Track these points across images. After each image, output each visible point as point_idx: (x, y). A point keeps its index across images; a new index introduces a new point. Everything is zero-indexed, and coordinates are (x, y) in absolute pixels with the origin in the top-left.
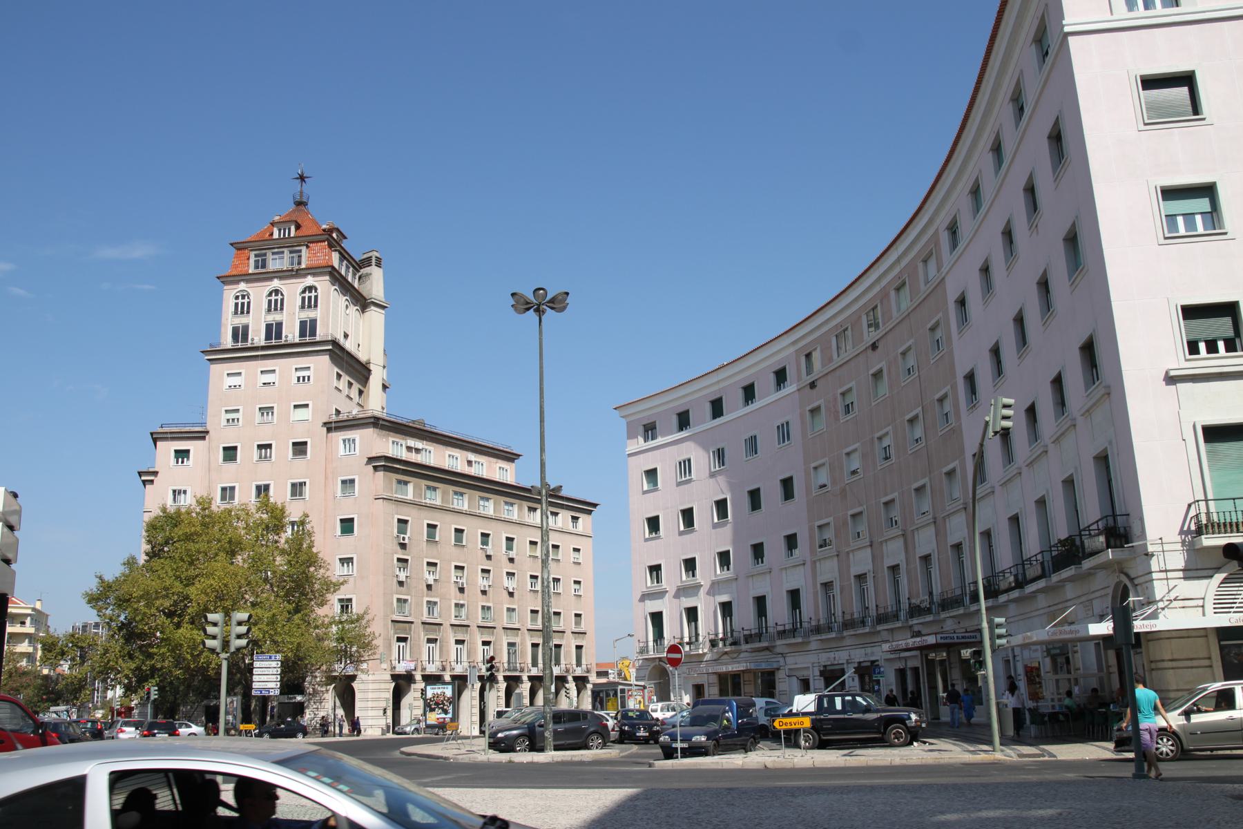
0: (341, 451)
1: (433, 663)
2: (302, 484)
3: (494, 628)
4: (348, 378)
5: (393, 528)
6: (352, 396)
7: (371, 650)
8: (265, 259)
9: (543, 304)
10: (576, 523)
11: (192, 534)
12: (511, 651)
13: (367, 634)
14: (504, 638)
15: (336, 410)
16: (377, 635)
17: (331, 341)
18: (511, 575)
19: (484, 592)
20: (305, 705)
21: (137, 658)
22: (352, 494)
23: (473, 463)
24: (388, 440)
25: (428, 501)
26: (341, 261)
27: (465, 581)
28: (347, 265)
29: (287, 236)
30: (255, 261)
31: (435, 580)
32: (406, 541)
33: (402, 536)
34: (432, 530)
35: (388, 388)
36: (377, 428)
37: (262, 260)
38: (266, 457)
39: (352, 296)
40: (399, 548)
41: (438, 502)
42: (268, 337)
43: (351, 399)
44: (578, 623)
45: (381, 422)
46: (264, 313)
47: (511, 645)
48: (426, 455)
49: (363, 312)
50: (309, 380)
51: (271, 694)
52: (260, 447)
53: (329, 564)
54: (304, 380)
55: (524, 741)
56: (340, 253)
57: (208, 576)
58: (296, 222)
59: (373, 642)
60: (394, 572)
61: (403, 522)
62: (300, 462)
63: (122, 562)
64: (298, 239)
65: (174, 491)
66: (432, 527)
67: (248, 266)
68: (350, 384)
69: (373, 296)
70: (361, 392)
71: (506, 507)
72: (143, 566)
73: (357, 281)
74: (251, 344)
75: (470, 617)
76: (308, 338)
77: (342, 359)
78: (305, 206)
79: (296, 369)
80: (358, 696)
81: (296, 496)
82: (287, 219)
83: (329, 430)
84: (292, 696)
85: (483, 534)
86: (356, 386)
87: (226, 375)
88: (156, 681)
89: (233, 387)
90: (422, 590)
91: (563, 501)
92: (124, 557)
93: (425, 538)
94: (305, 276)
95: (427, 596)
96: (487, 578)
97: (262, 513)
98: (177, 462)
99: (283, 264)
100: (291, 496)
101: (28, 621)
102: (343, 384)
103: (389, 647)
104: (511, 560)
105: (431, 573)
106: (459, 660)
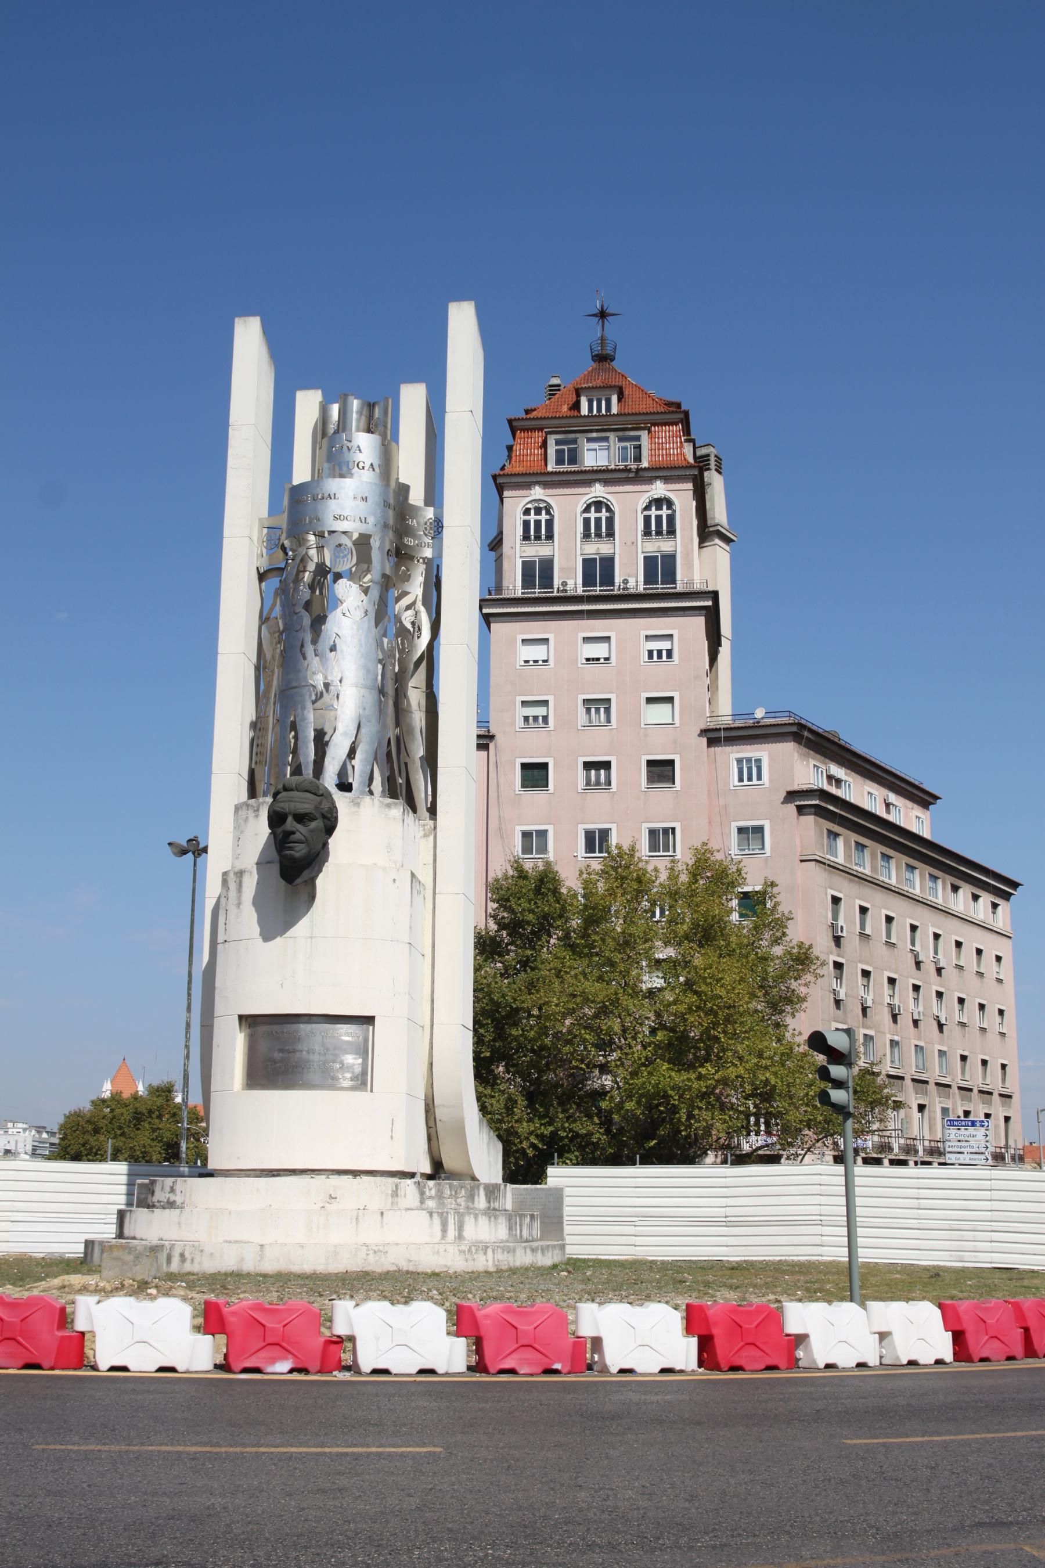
8: (575, 450)
24: (808, 765)
30: (557, 451)
37: (569, 450)
38: (598, 783)
45: (806, 734)
52: (588, 766)
54: (660, 656)
60: (831, 985)
62: (662, 795)
64: (623, 418)
79: (646, 636)
81: (595, 852)
83: (712, 742)
87: (519, 642)
89: (531, 663)
94: (650, 480)
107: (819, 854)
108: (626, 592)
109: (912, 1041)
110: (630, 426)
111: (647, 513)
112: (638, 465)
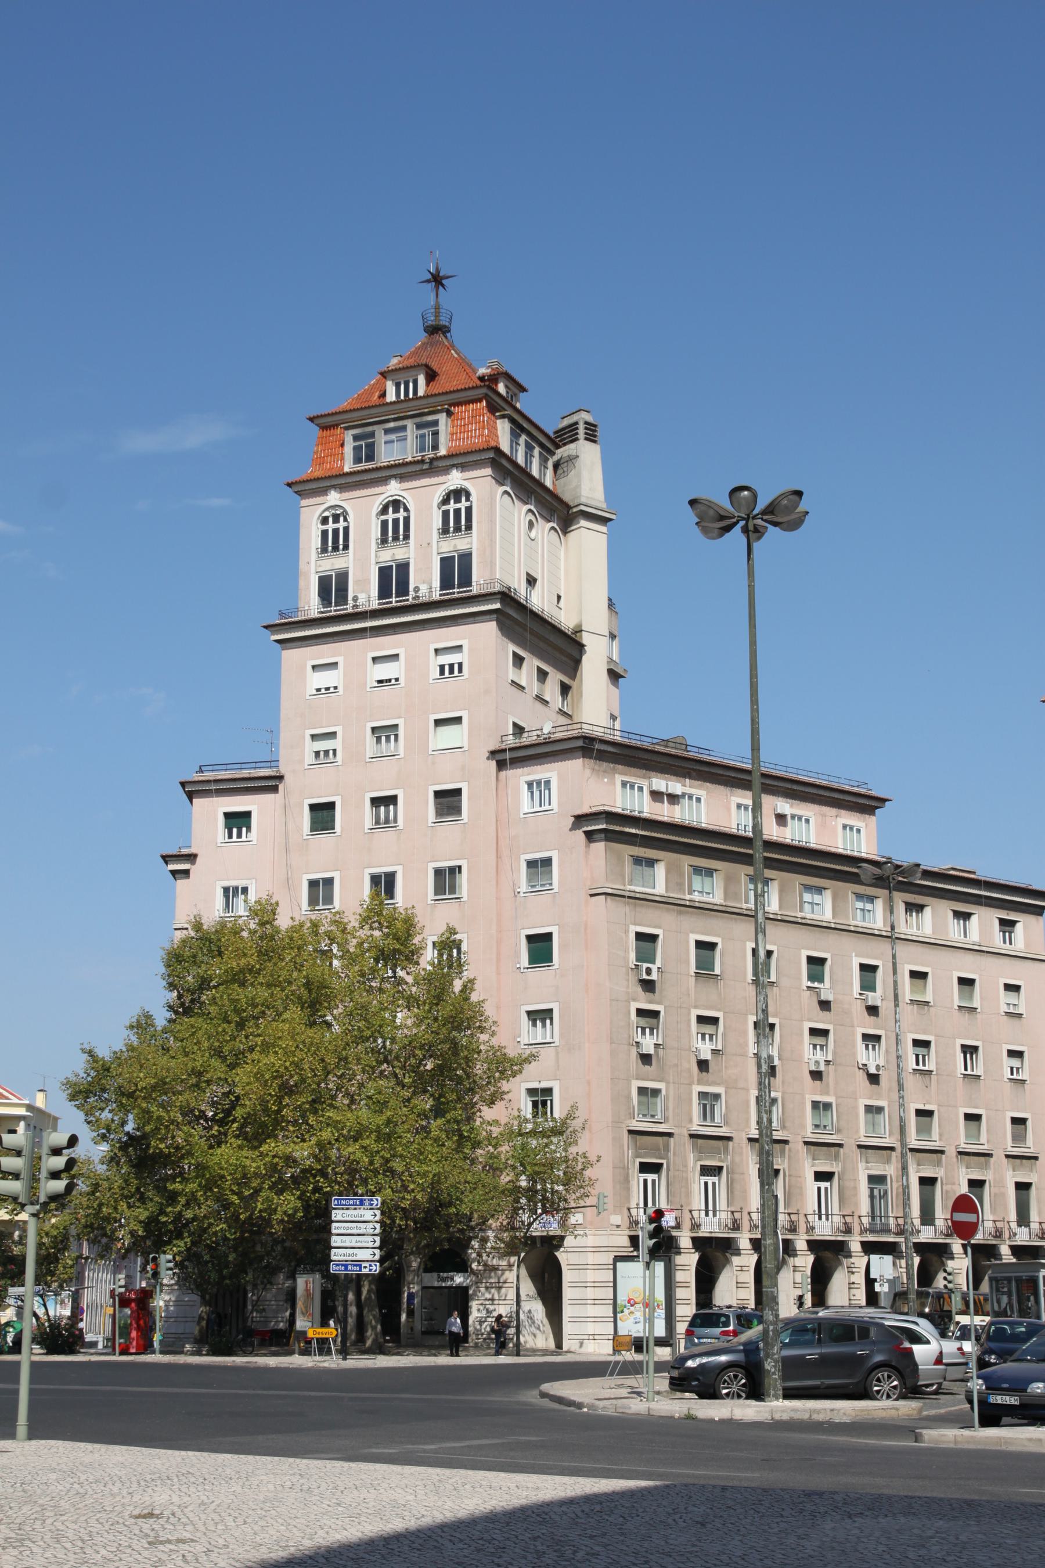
0: (525, 804)
1: (714, 1215)
2: (455, 871)
3: (840, 1145)
4: (537, 663)
5: (627, 951)
6: (547, 698)
7: (581, 1187)
9: (754, 518)
10: (1010, 933)
11: (242, 971)
12: (876, 1192)
13: (571, 1157)
14: (861, 1166)
15: (515, 725)
16: (593, 1158)
17: (499, 593)
18: (871, 1039)
19: (816, 1075)
20: (471, 1292)
21: (151, 1200)
22: (548, 887)
23: (789, 818)
25: (696, 897)
26: (515, 435)
27: (775, 1054)
28: (527, 443)
29: (411, 396)
30: (355, 448)
31: (715, 1052)
32: (654, 976)
33: (645, 965)
34: (705, 953)
35: (622, 677)
36: (591, 758)
38: (387, 821)
39: (541, 503)
40: (639, 989)
41: (717, 898)
42: (384, 592)
43: (546, 703)
44: (1019, 1138)
45: (597, 746)
46: (374, 546)
47: (876, 1180)
48: (690, 807)
49: (565, 532)
50: (460, 670)
51: (365, 1271)
52: (376, 802)
53: (495, 1022)
54: (451, 671)
55: (736, 1376)
56: (512, 421)
57: (266, 1048)
58: (427, 366)
59: (587, 1173)
61: (646, 939)
62: (450, 829)
63: (128, 1025)
65: (226, 890)
66: (706, 947)
67: (342, 459)
68: (542, 675)
69: (583, 500)
70: (565, 689)
71: (860, 905)
72: (165, 1031)
73: (550, 472)
74: (414, 598)
75: (787, 1124)
76: (394, 599)
77: (523, 626)
78: (444, 333)
80: (567, 1276)
82: (411, 362)
83: (501, 765)
84: (445, 1275)
85: (811, 960)
86: (555, 677)
87: (309, 669)
88: (186, 1243)
89: (323, 691)
90: (689, 1071)
91: (980, 889)
92: (131, 1015)
93: (693, 969)
94: (446, 470)
95: (700, 1082)
96: (822, 1046)
97: (372, 928)
98: (230, 836)
99: (404, 450)
100: (436, 894)
101: (21, 1127)
102: (527, 675)
103: (625, 1181)
104: (873, 1010)
105: (707, 1036)
106: (823, 1211)
107: (610, 887)
108: (417, 602)
109: (807, 1096)
110: (426, 410)
111: (445, 508)
112: (435, 454)
